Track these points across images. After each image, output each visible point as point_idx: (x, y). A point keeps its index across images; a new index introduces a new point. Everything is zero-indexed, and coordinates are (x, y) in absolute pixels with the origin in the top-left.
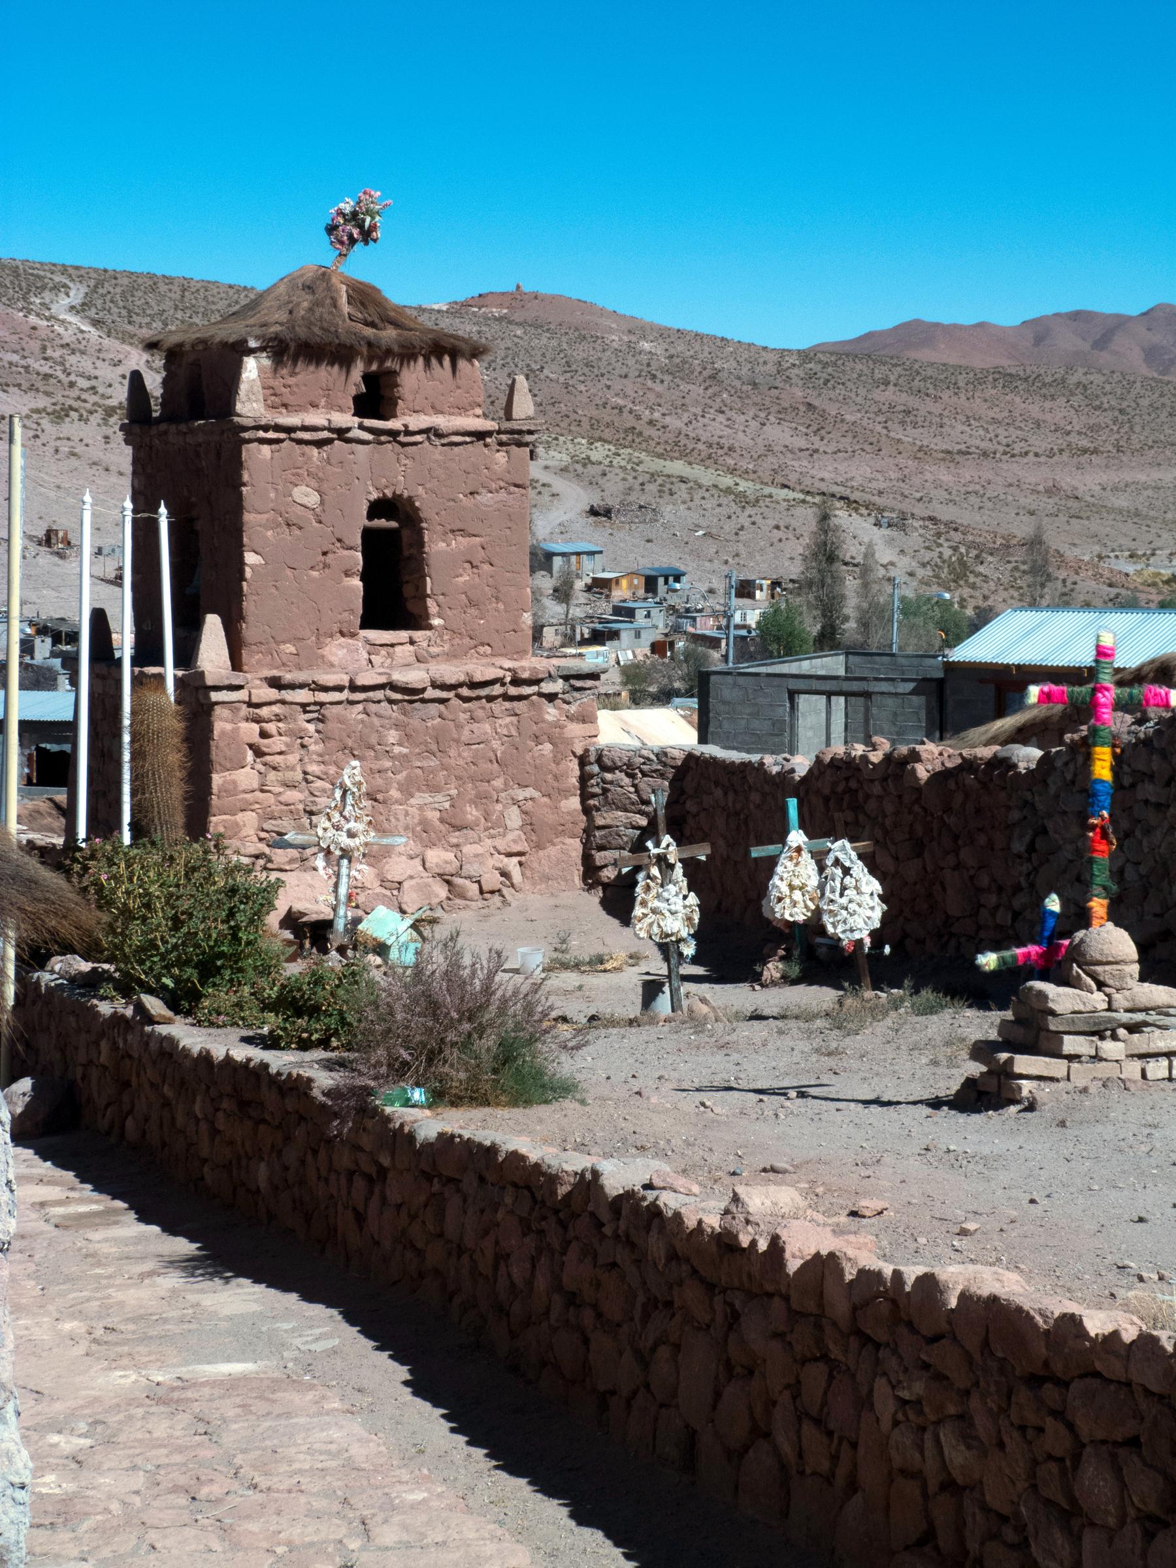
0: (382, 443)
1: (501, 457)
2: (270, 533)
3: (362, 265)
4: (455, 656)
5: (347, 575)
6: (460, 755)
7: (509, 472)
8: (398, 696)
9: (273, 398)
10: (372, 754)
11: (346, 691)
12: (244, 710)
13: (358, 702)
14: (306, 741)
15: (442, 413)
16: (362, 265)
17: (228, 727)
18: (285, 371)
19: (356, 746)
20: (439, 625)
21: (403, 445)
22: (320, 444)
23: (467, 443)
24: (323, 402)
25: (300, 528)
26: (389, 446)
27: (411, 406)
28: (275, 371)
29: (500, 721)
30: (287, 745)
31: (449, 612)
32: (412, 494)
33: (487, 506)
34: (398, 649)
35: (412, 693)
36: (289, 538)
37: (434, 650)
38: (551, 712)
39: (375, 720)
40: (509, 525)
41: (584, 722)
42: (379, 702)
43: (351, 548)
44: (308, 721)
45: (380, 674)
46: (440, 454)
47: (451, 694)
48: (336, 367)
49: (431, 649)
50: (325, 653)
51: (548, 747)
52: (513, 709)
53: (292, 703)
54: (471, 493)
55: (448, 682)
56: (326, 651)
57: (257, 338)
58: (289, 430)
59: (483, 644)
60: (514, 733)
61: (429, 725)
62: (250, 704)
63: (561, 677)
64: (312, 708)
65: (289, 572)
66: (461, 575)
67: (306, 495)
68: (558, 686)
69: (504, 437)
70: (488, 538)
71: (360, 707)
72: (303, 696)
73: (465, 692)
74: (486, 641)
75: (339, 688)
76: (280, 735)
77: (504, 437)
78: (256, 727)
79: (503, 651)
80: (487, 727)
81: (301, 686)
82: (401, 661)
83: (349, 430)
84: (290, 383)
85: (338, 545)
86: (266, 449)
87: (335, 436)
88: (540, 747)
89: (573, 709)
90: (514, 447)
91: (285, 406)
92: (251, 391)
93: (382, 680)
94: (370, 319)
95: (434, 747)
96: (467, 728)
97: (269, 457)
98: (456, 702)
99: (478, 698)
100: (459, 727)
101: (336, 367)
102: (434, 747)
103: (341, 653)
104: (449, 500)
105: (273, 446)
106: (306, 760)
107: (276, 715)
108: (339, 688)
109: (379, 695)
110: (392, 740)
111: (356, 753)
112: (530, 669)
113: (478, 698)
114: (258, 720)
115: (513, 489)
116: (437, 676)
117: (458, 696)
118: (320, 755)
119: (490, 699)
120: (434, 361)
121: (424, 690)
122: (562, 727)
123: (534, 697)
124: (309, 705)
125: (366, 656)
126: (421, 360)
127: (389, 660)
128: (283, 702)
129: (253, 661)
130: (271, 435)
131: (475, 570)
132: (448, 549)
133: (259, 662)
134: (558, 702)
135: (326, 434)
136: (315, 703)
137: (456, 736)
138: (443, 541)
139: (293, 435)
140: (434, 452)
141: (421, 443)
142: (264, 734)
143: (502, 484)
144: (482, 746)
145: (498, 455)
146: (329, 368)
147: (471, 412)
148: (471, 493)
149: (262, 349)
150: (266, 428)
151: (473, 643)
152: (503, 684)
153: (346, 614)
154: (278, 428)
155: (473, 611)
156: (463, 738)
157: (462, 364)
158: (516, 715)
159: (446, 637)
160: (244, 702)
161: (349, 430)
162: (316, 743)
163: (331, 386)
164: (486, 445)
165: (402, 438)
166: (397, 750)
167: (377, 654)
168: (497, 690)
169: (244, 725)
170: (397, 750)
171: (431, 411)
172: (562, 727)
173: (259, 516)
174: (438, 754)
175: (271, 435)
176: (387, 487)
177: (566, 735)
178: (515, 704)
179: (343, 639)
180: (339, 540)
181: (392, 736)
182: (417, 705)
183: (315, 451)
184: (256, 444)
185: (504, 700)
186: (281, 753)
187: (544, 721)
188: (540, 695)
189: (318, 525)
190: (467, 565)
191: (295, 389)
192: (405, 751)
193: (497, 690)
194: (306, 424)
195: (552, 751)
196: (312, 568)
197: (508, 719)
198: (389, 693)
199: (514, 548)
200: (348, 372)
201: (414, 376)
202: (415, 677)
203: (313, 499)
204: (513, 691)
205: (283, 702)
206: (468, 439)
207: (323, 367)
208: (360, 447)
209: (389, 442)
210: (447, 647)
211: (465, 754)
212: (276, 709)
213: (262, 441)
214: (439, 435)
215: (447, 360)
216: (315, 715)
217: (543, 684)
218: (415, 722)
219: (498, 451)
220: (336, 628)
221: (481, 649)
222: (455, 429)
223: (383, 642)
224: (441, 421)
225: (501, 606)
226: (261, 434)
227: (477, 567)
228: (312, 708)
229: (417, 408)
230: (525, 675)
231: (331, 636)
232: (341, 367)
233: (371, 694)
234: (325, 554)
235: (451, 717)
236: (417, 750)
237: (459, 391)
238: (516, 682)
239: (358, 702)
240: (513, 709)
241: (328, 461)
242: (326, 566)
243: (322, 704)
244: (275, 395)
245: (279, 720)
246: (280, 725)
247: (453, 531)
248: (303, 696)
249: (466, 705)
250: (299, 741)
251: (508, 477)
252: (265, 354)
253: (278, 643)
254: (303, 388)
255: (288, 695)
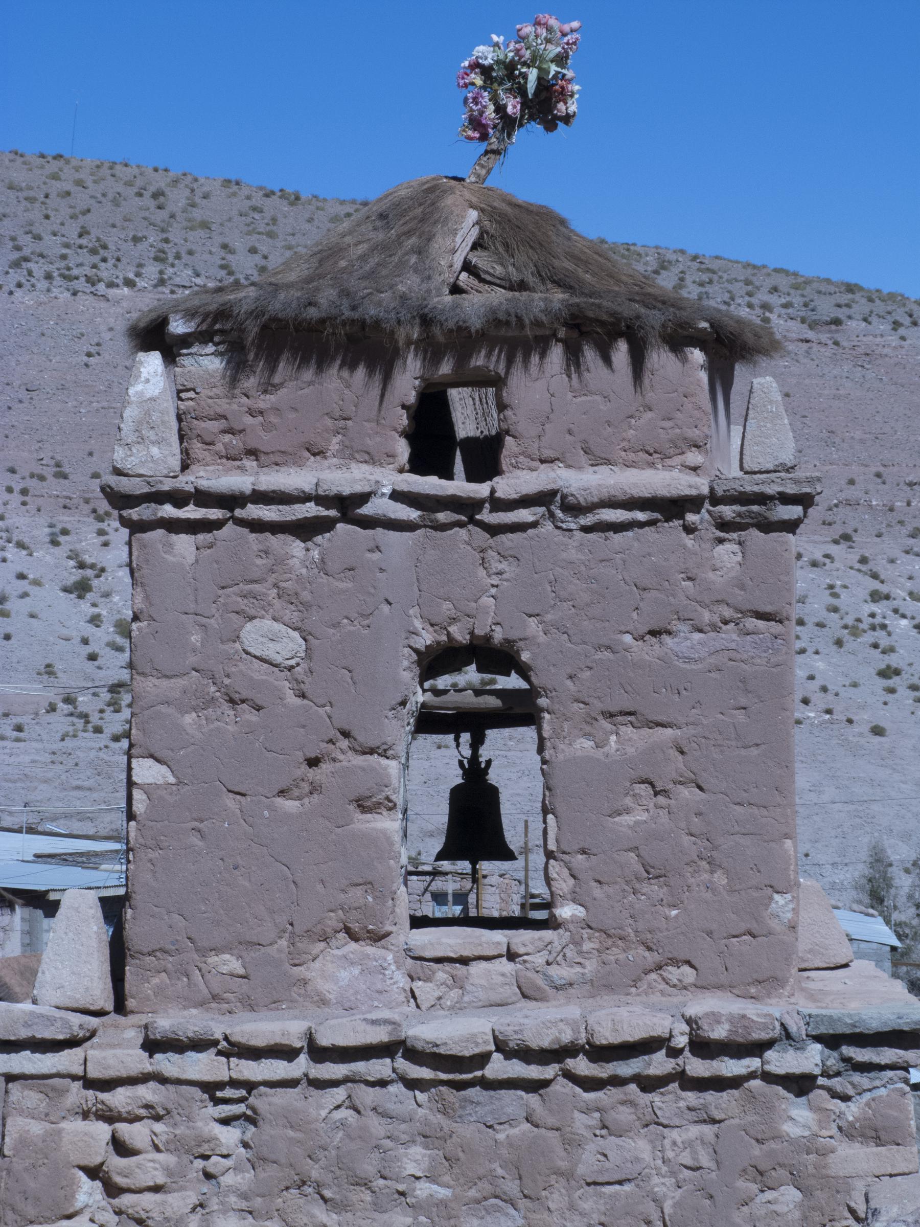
0: (442, 527)
1: (727, 554)
2: (189, 719)
3: (534, 169)
4: (609, 988)
5: (364, 809)
6: (572, 1207)
7: (742, 587)
8: (425, 1073)
9: (227, 438)
10: (367, 1197)
11: (303, 1058)
12: (76, 1094)
13: (335, 1083)
14: (215, 1164)
15: (608, 462)
16: (534, 169)
17: (37, 1128)
18: (250, 383)
19: (328, 1178)
20: (574, 920)
21: (494, 530)
22: (304, 530)
23: (641, 525)
24: (335, 443)
25: (258, 709)
26: (462, 533)
27: (534, 449)
28: (233, 382)
29: (674, 1134)
30: (169, 1172)
31: (597, 892)
32: (513, 635)
33: (688, 660)
34: (477, 968)
35: (457, 1070)
36: (231, 728)
37: (560, 973)
38: (798, 1117)
39: (377, 1126)
40: (743, 701)
41: (879, 1141)
42: (382, 1083)
43: (371, 751)
44: (225, 1121)
45: (374, 1022)
46: (580, 547)
47: (549, 1071)
48: (361, 372)
49: (555, 972)
50: (309, 975)
51: (789, 1196)
52: (705, 1107)
53: (179, 1082)
54: (654, 633)
55: (534, 1044)
56: (312, 971)
57: (190, 314)
58: (230, 501)
59: (676, 962)
60: (705, 1160)
61: (501, 1137)
62: (90, 1084)
63: (818, 1039)
64: (228, 1093)
65: (231, 802)
66: (628, 811)
67: (272, 638)
68: (810, 1059)
69: (728, 511)
70: (691, 731)
71: (340, 1094)
72: (202, 1066)
73: (581, 1066)
74: (682, 956)
75: (287, 1053)
76: (157, 1149)
77: (728, 511)
78: (103, 1130)
79: (724, 978)
80: (640, 1146)
81: (199, 1045)
82: (481, 995)
83: (364, 498)
84: (262, 405)
85: (344, 743)
86: (184, 543)
87: (333, 513)
88: (769, 1195)
89: (852, 1111)
90: (754, 533)
91: (253, 453)
92: (145, 421)
93: (380, 1035)
94: (515, 276)
95: (511, 1187)
96: (591, 1147)
97: (191, 559)
98: (563, 1087)
99: (617, 1081)
100: (572, 1143)
101: (361, 372)
102: (511, 1187)
103: (345, 975)
104: (599, 648)
105: (201, 537)
106: (214, 1204)
107: (147, 1106)
108: (287, 1053)
109: (380, 1068)
110: (411, 1168)
111: (328, 1193)
112: (731, 1019)
113: (617, 1081)
114: (109, 1117)
115: (752, 623)
116: (509, 1030)
117: (569, 1076)
118: (245, 1197)
119: (649, 1084)
120: (590, 355)
121: (482, 1059)
122: (823, 1153)
123: (755, 1083)
124: (220, 1085)
125: (403, 982)
126: (556, 353)
127: (455, 994)
128: (163, 1080)
129: (147, 989)
130: (191, 512)
131: (661, 799)
132: (599, 754)
133: (159, 991)
134: (818, 1095)
135: (311, 510)
136: (234, 1083)
137: (563, 1164)
138: (587, 735)
139: (238, 513)
140: (563, 546)
141: (534, 525)
142: (121, 1148)
143: (728, 613)
144: (627, 1187)
145: (720, 548)
146: (345, 374)
147: (677, 460)
148: (654, 633)
149: (203, 337)
150: (178, 499)
151: (651, 958)
152: (674, 1053)
153: (359, 892)
154: (203, 498)
155: (654, 889)
156: (581, 1170)
157: (660, 359)
158: (714, 1121)
159: (587, 946)
160: (74, 1078)
161: (364, 498)
162: (236, 1169)
163: (350, 410)
164: (689, 530)
165: (486, 516)
166: (424, 1189)
167: (428, 980)
168: (658, 1064)
169: (78, 1125)
170: (424, 1189)
171: (583, 458)
172: (823, 1153)
173: (165, 683)
174: (522, 1203)
175: (191, 512)
176: (454, 620)
177: (832, 1172)
178: (710, 1097)
179: (353, 945)
180: (346, 734)
181: (414, 1159)
182: (474, 1092)
183: (296, 547)
184: (160, 532)
185: (683, 1088)
186: (156, 1189)
187: (777, 1137)
188: (769, 1078)
189: (299, 701)
190: (643, 790)
191: (273, 419)
192: (442, 1193)
193: (658, 1064)
194: (262, 487)
195: (799, 1206)
196: (282, 793)
197: (694, 1131)
198: (401, 1063)
199: (754, 752)
200: (387, 379)
201: (541, 385)
202: (455, 1030)
203: (287, 645)
204: (697, 1067)
205: (163, 1080)
206: (641, 516)
207: (334, 370)
208: (393, 536)
209: (461, 525)
210: (591, 966)
211: (586, 1206)
212: (147, 1092)
213: (174, 526)
214: (574, 509)
215: (621, 352)
216: (240, 1108)
217: (769, 1054)
218: (467, 1131)
219: (721, 541)
220: (333, 921)
221: (673, 973)
222: (605, 495)
223: (440, 954)
224: (581, 480)
225: (720, 879)
226: (168, 511)
227: (665, 792)
228: (228, 1093)
229: (548, 453)
230: (719, 1033)
231: (326, 939)
232: (371, 372)
233: (360, 1067)
234: (313, 762)
235: (551, 1121)
236: (473, 1193)
237: (649, 415)
238: (703, 1047)
239: (335, 1083)
240: (705, 1107)
241: (322, 566)
242: (315, 789)
243: (250, 1086)
244: (230, 431)
245: (157, 1118)
246: (159, 1127)
247: (610, 715)
248: (202, 1066)
249: (592, 1096)
250: (199, 1164)
251: (739, 597)
252: (210, 348)
253: (204, 952)
254: (292, 415)
255: (168, 1063)
